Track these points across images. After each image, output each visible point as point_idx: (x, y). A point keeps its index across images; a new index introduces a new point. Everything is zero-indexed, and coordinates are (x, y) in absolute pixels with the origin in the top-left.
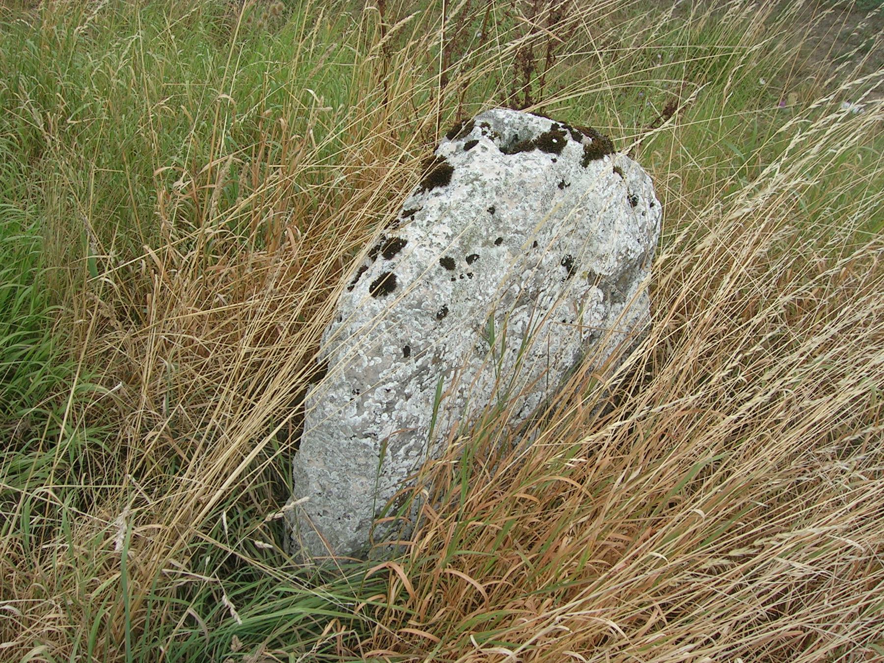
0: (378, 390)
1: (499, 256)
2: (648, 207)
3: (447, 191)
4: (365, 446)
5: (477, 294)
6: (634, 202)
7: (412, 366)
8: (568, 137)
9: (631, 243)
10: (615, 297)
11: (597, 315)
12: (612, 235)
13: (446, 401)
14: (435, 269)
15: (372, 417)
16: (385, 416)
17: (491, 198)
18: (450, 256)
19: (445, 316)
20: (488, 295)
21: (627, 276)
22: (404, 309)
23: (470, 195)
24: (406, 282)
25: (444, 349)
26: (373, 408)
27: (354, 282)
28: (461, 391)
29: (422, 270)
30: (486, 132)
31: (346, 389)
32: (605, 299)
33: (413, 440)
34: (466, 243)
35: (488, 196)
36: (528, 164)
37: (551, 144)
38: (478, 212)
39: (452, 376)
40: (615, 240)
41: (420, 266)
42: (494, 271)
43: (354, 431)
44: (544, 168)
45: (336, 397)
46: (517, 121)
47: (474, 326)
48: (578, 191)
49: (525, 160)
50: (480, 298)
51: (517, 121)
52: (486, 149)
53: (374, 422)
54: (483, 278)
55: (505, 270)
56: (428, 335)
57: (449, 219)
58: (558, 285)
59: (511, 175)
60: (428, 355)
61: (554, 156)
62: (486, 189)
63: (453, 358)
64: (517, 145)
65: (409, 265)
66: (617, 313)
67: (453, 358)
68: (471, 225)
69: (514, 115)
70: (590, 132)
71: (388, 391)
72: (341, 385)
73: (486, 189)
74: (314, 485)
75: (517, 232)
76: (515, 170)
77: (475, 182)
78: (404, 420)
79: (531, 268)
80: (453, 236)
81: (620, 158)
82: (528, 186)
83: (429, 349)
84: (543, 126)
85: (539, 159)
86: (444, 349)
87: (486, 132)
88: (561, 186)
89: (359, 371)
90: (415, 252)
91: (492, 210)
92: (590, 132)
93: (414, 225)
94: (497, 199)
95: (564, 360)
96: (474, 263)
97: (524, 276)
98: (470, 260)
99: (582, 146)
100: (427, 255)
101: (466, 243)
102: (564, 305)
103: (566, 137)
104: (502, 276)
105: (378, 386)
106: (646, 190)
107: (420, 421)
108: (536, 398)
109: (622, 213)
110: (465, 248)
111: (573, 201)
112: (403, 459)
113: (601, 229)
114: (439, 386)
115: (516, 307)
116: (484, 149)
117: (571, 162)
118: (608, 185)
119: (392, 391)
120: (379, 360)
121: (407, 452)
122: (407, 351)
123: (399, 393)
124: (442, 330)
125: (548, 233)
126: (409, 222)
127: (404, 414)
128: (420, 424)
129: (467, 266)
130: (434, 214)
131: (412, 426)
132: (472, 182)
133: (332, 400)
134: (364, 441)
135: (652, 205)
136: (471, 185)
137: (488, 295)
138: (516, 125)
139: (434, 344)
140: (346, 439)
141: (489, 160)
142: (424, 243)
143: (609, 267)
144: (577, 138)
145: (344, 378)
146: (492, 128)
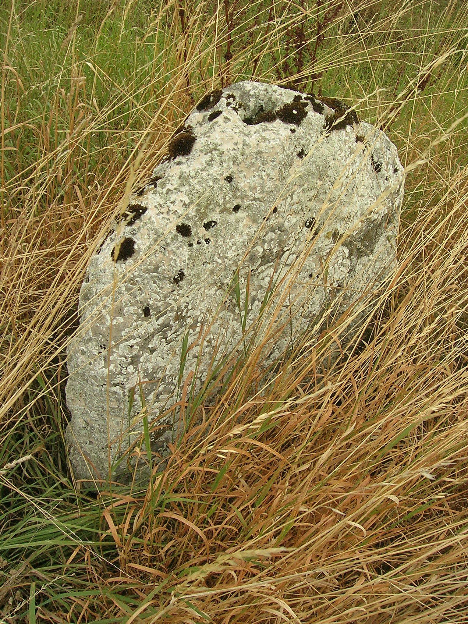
0: (121, 346)
1: (238, 221)
2: (391, 172)
3: (188, 160)
4: (115, 393)
5: (216, 258)
6: (377, 168)
7: (154, 324)
8: (309, 109)
9: (373, 205)
10: (361, 252)
11: (343, 268)
12: (356, 199)
13: (196, 350)
14: (170, 236)
15: (118, 370)
16: (131, 368)
17: (229, 167)
18: (187, 223)
19: (182, 279)
20: (227, 258)
21: (372, 234)
22: (142, 273)
23: (208, 164)
24: (143, 247)
25: (186, 307)
26: (119, 362)
27: (101, 245)
28: (209, 341)
29: (159, 236)
30: (230, 103)
31: (95, 343)
32: (351, 254)
33: (163, 386)
34: (202, 210)
35: (225, 165)
36: (266, 134)
37: (292, 115)
38: (215, 180)
39: (198, 329)
40: (358, 204)
41: (156, 233)
42: (232, 237)
43: (104, 380)
44: (282, 138)
45: (86, 350)
46: (262, 92)
47: (219, 284)
48: (318, 160)
49: (264, 130)
50: (220, 261)
51: (262, 92)
52: (229, 119)
53: (120, 373)
54: (220, 243)
55: (244, 234)
56: (166, 297)
57: (187, 188)
58: (303, 245)
59: (249, 145)
60: (169, 314)
61: (293, 126)
62: (223, 159)
63: (199, 313)
64: (261, 116)
65: (147, 232)
66: (364, 265)
67: (199, 313)
68: (208, 194)
69: (260, 87)
70: (333, 104)
71: (132, 347)
72: (90, 340)
73: (223, 159)
74: (79, 420)
75: (255, 199)
76: (252, 140)
77: (213, 152)
78: (150, 371)
79: (273, 231)
80: (190, 204)
81: (364, 127)
82: (265, 155)
83: (169, 309)
84: (287, 97)
85: (280, 129)
86: (186, 307)
87: (230, 103)
88: (301, 155)
89: (103, 328)
90: (153, 219)
91: (229, 179)
92: (333, 104)
93: (155, 193)
94: (234, 168)
95: (311, 309)
96: (211, 229)
97: (266, 239)
98: (207, 226)
99: (324, 117)
100: (164, 222)
101: (202, 210)
102: (311, 263)
103: (307, 109)
104: (241, 240)
105: (121, 343)
106: (390, 155)
107: (168, 370)
108: (285, 342)
109: (366, 178)
110: (202, 216)
111: (313, 169)
112: (155, 402)
113: (344, 194)
114: (186, 339)
115: (261, 265)
116: (227, 119)
117: (311, 132)
118: (350, 154)
119: (135, 347)
120: (121, 319)
121: (157, 396)
122: (147, 312)
123: (143, 348)
124: (180, 292)
125: (289, 199)
126: (152, 189)
127: (150, 366)
128: (167, 373)
129: (205, 232)
130: (175, 182)
131: (160, 375)
132: (211, 152)
133: (83, 353)
134: (114, 389)
135: (396, 171)
136: (210, 154)
137: (227, 258)
138: (262, 97)
139: (175, 305)
140: (98, 386)
141: (228, 130)
142: (163, 211)
143: (354, 227)
144: (318, 109)
145: (91, 334)
146: (237, 99)
